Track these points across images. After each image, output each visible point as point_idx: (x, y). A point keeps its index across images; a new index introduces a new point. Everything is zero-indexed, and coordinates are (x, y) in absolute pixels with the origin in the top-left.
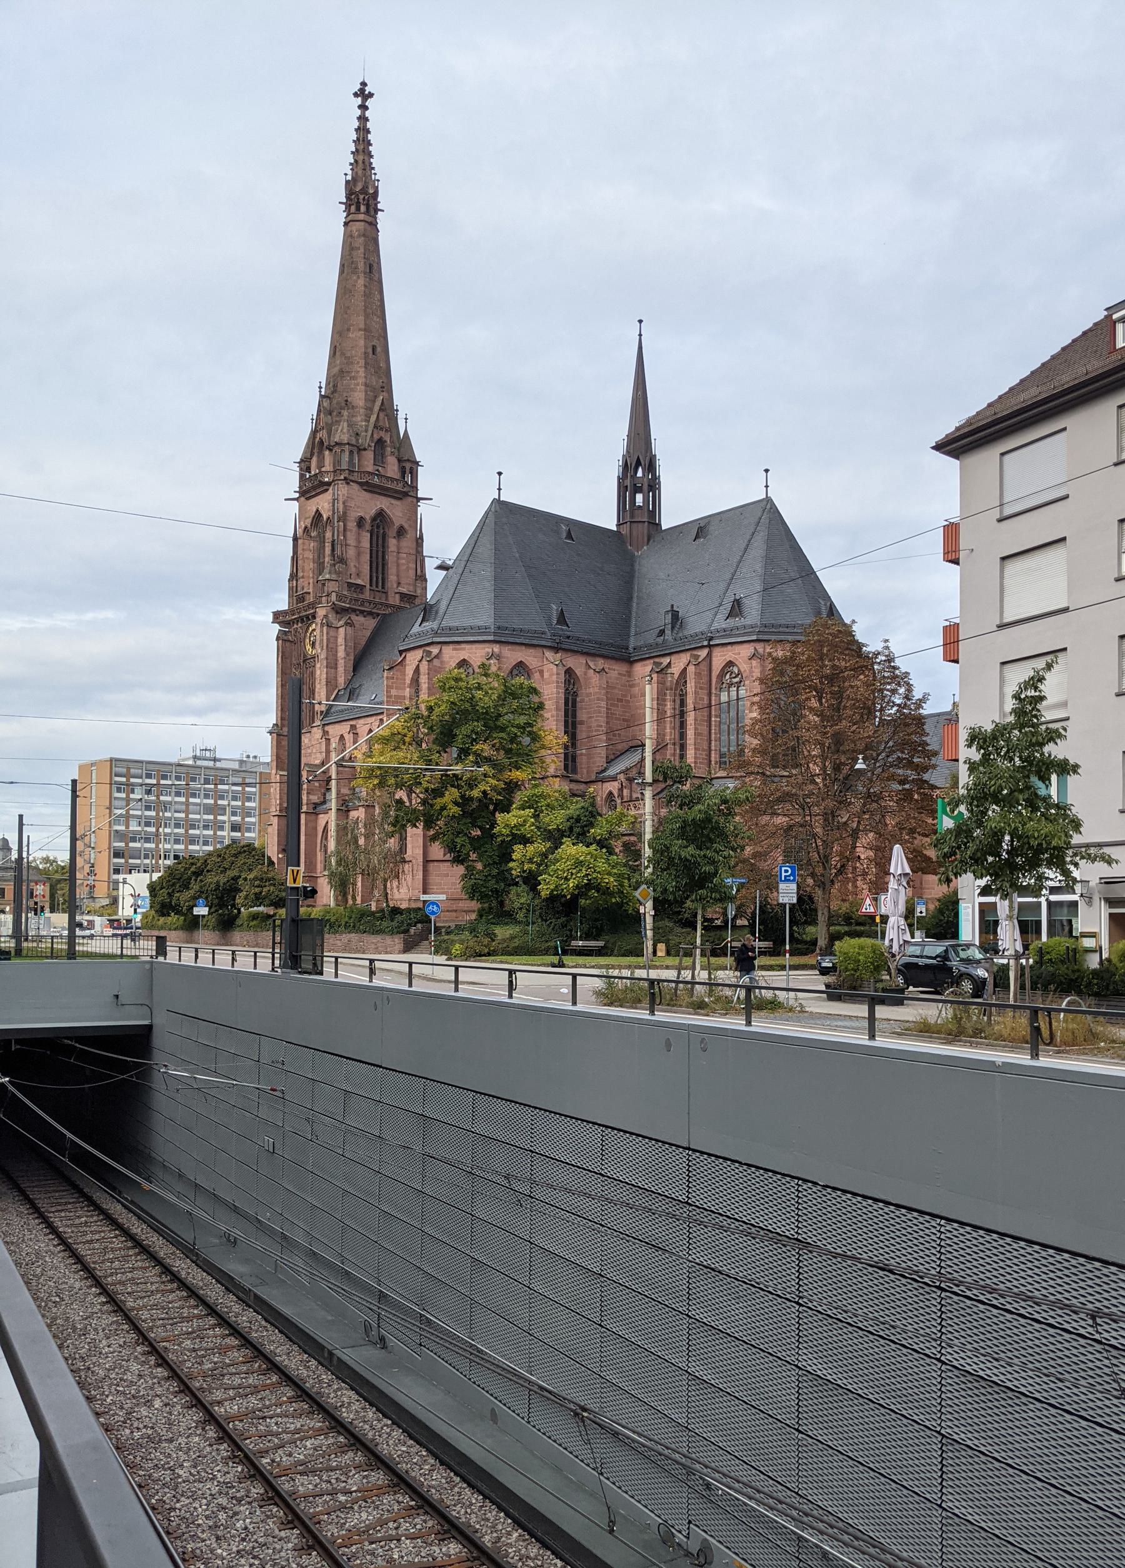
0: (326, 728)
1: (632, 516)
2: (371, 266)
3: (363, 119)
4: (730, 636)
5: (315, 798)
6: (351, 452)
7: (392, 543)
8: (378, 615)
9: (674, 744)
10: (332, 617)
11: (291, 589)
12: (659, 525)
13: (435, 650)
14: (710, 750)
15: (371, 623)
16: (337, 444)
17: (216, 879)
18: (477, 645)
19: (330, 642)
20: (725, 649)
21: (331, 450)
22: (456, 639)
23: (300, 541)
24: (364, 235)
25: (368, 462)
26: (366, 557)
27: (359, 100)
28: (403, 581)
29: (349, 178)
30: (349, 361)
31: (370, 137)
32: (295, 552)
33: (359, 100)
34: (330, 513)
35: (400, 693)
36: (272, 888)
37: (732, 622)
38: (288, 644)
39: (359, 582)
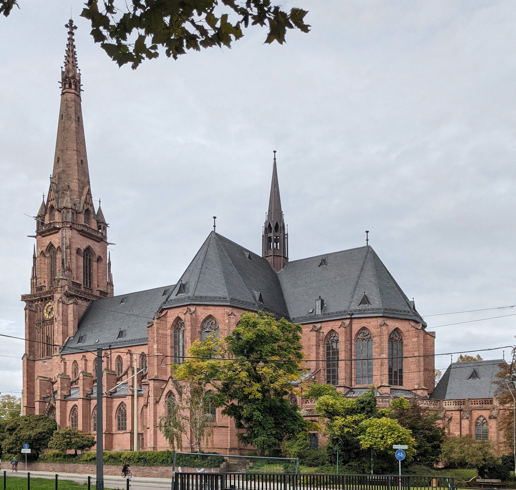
0: (63, 357)
1: (274, 253)
2: (78, 118)
3: (71, 40)
4: (362, 314)
6: (73, 213)
7: (95, 264)
8: (89, 300)
9: (324, 370)
10: (64, 299)
12: (287, 259)
13: (193, 309)
15: (85, 304)
16: (64, 208)
17: (28, 433)
19: (61, 313)
20: (360, 320)
22: (206, 303)
23: (38, 259)
24: (74, 101)
27: (68, 30)
28: (101, 285)
29: (64, 70)
30: (68, 166)
32: (35, 264)
33: (68, 30)
34: (60, 245)
35: (164, 332)
36: (78, 439)
37: (362, 307)
38: (32, 312)
39: (78, 282)
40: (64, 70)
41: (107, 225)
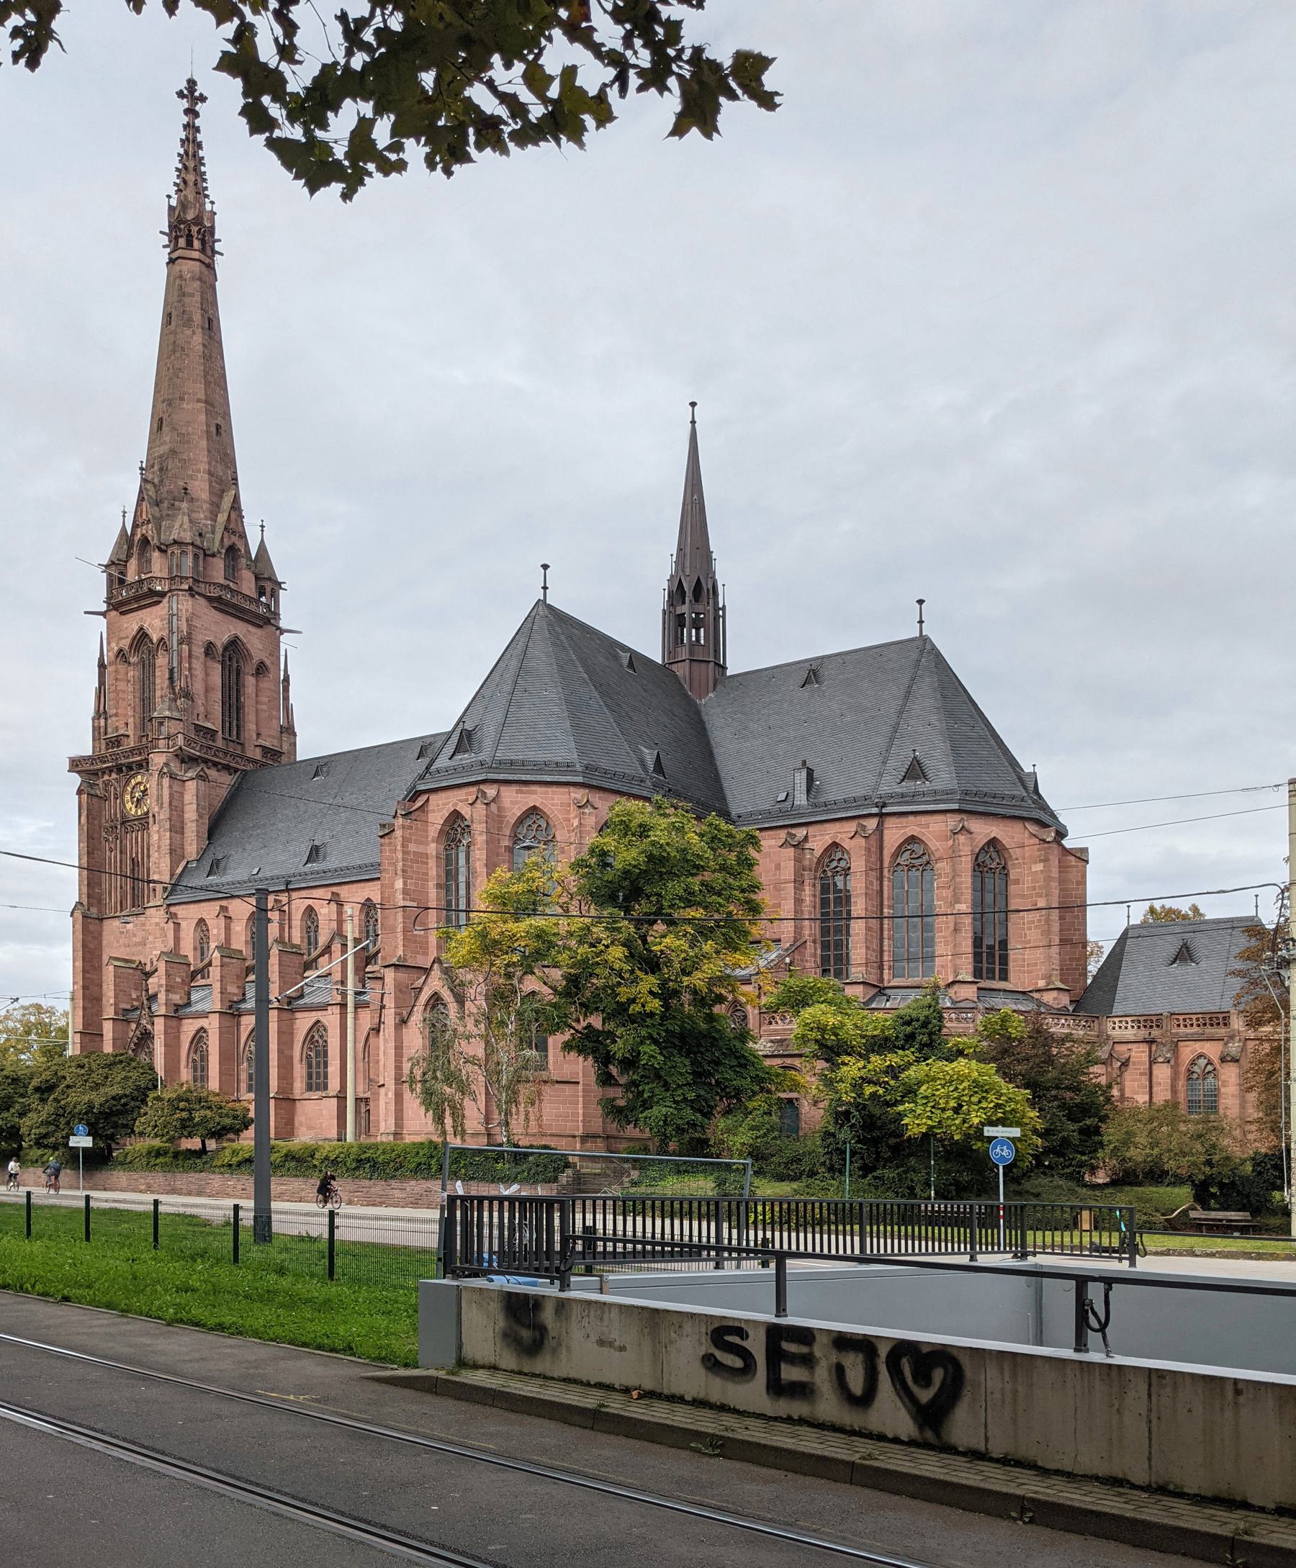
0: (173, 909)
1: (691, 653)
2: (210, 321)
3: (191, 128)
5: (177, 998)
7: (250, 681)
8: (236, 770)
9: (814, 942)
10: (175, 766)
11: (96, 729)
12: (724, 668)
13: (491, 791)
14: (882, 951)
15: (227, 780)
16: (175, 542)
17: (87, 1098)
18: (554, 789)
19: (168, 804)
20: (904, 820)
21: (164, 552)
22: (524, 778)
23: (110, 669)
24: (200, 279)
25: (218, 570)
26: (218, 695)
27: (185, 104)
28: (264, 732)
29: (174, 202)
31: (201, 153)
34: (165, 633)
35: (421, 849)
36: (208, 1113)
37: (909, 786)
38: (95, 800)
39: (209, 725)
40: (174, 202)
41: (280, 584)
